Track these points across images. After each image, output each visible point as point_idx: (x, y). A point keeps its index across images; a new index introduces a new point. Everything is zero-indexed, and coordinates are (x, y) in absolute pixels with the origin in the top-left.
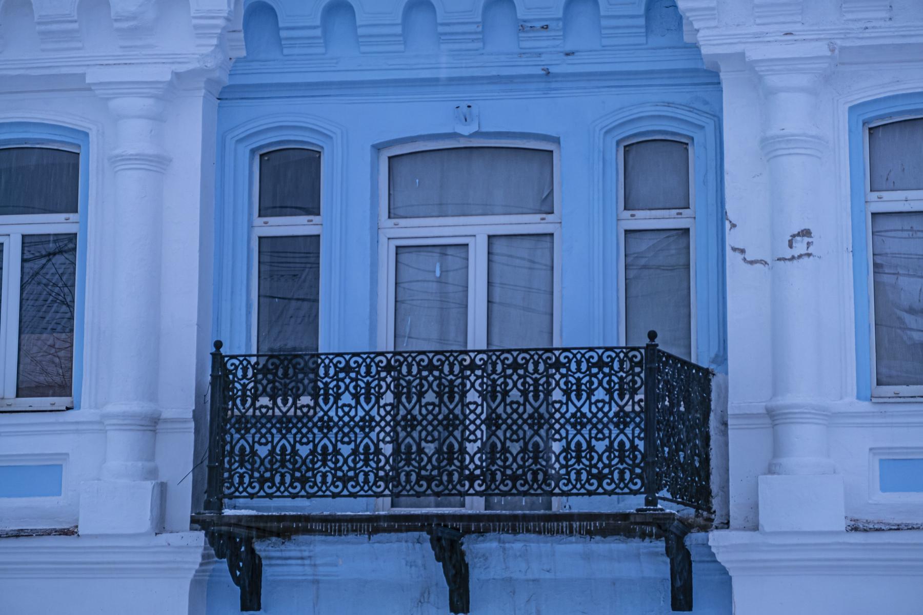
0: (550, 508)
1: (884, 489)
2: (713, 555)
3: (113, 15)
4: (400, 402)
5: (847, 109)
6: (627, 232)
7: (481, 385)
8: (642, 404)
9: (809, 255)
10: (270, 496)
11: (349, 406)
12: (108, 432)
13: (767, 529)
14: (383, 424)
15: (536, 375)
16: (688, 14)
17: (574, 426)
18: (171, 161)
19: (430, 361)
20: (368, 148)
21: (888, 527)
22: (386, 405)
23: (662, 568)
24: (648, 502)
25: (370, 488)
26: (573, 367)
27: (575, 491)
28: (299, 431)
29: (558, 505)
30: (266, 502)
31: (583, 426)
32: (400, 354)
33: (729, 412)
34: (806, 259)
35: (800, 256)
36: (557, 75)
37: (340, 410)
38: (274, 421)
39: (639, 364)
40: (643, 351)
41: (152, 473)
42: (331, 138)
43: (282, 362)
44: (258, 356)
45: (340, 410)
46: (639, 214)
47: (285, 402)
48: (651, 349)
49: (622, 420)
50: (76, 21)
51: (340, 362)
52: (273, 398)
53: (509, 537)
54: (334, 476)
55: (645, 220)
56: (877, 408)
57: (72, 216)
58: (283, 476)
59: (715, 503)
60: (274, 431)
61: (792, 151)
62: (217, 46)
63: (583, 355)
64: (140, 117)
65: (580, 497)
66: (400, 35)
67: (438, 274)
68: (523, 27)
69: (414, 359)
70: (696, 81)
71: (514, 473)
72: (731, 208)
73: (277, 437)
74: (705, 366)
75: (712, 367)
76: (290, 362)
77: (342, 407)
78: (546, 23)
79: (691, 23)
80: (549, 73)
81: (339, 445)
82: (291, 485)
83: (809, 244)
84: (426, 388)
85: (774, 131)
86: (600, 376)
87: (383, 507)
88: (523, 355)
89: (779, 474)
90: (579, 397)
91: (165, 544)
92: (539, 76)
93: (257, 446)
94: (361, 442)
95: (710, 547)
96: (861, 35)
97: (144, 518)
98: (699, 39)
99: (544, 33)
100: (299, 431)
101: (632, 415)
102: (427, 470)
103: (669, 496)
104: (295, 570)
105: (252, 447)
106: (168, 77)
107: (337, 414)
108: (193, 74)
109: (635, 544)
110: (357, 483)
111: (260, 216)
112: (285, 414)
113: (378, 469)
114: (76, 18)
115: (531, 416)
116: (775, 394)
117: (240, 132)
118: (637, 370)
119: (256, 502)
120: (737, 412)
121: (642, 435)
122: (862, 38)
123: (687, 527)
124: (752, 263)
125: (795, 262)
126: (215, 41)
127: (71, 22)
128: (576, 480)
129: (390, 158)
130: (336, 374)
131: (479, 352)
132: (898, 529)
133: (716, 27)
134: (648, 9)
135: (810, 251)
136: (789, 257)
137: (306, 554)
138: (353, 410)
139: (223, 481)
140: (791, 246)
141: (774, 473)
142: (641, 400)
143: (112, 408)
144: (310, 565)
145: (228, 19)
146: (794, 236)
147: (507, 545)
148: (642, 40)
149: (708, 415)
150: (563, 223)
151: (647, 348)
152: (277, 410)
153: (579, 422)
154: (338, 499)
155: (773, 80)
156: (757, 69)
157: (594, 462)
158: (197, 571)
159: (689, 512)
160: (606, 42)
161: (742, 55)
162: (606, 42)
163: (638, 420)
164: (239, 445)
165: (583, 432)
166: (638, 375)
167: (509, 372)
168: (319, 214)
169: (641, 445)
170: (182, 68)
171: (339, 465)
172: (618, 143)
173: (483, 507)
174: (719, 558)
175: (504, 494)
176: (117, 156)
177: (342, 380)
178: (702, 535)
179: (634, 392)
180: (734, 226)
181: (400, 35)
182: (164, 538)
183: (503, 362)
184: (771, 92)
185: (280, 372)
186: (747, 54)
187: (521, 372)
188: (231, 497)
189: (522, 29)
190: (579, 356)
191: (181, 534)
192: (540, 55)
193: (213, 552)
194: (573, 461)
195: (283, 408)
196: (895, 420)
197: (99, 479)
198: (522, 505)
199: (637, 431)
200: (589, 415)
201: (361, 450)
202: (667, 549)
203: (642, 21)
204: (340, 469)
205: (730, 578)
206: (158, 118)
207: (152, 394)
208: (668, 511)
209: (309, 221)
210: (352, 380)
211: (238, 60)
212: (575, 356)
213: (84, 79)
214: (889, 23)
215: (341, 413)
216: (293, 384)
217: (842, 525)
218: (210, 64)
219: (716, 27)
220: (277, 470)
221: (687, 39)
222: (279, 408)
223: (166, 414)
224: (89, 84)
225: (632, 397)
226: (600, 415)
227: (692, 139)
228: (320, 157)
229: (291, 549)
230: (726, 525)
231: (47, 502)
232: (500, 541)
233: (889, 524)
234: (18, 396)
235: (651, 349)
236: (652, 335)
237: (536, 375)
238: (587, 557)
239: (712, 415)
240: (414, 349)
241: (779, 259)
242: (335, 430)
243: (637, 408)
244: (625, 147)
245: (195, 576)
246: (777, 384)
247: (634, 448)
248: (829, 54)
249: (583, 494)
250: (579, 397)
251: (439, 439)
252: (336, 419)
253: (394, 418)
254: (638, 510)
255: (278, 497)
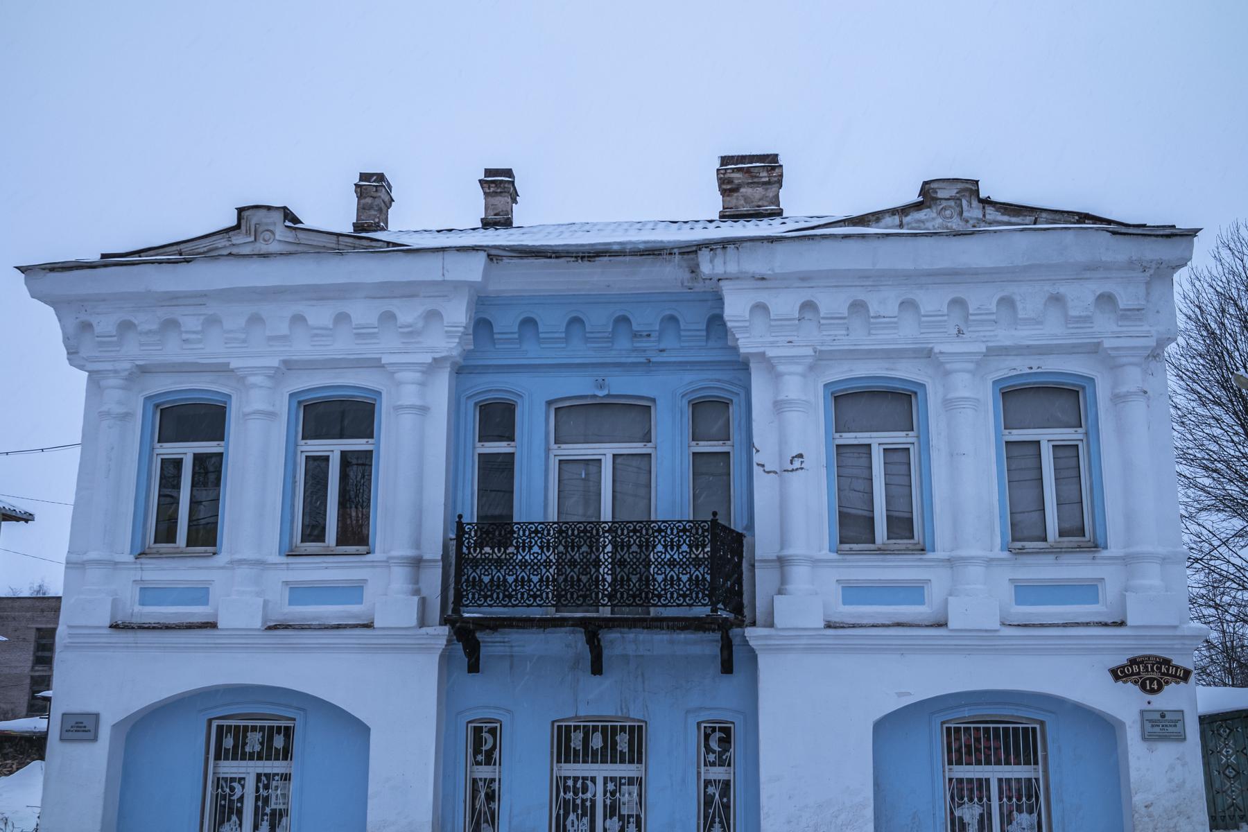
0: (649, 614)
1: (844, 603)
2: (747, 641)
3: (398, 324)
4: (617, 550)
5: (822, 386)
6: (694, 454)
7: (689, 541)
8: (709, 554)
9: (802, 468)
10: (490, 606)
11: (537, 553)
12: (392, 567)
13: (779, 626)
14: (631, 563)
15: (524, 538)
16: (732, 330)
17: (669, 566)
18: (429, 409)
19: (585, 527)
20: (544, 403)
21: (847, 626)
22: (608, 552)
23: (715, 649)
24: (712, 611)
25: (476, 602)
26: (669, 531)
27: (670, 604)
28: (508, 568)
29: (653, 612)
30: (489, 609)
31: (675, 566)
32: (617, 522)
33: (756, 558)
34: (800, 471)
35: (797, 469)
36: (654, 363)
37: (606, 555)
38: (493, 562)
39: (707, 530)
40: (709, 523)
41: (417, 592)
42: (521, 396)
43: (497, 527)
44: (613, 522)
45: (606, 555)
46: (701, 443)
47: (499, 551)
48: (714, 522)
49: (697, 562)
50: (376, 328)
51: (532, 528)
52: (492, 548)
53: (626, 630)
54: (528, 594)
55: (705, 447)
56: (841, 557)
57: (371, 441)
58: (498, 594)
59: (746, 611)
60: (493, 567)
61: (794, 409)
62: (458, 343)
63: (674, 525)
64: (413, 383)
65: (673, 608)
66: (517, 339)
67: (583, 476)
68: (636, 335)
69: (575, 526)
70: (736, 367)
71: (486, 593)
72: (756, 441)
73: (544, 570)
74: (740, 532)
75: (744, 532)
76: (502, 527)
77: (533, 554)
78: (648, 333)
79: (734, 335)
80: (650, 361)
81: (531, 576)
82: (503, 599)
83: (802, 462)
84: (533, 544)
85: (782, 397)
86: (685, 537)
87: (551, 612)
88: (639, 525)
89: (785, 594)
90: (524, 551)
91: (425, 633)
92: (645, 363)
93: (483, 576)
94: (694, 573)
95: (745, 637)
96: (832, 344)
97: (413, 621)
98: (739, 344)
99: (649, 339)
100: (508, 568)
101: (703, 560)
102: (583, 591)
103: (723, 607)
104: (498, 650)
105: (480, 577)
106: (430, 361)
107: (530, 558)
108: (444, 359)
109: (699, 635)
110: (542, 599)
111: (479, 441)
112: (499, 558)
113: (530, 590)
114: (995, 311)
115: (569, 561)
116: (782, 548)
117: (469, 393)
118: (706, 534)
119: (483, 609)
120: (760, 558)
121: (709, 572)
122: (831, 346)
123: (732, 625)
124: (769, 472)
125: (794, 473)
126: (457, 340)
127: (111, 336)
128: (645, 598)
129: (556, 409)
130: (530, 534)
131: (689, 522)
132: (853, 627)
133: (748, 337)
134: (708, 326)
135: (802, 466)
136: (790, 469)
137: (506, 640)
138: (540, 556)
139: (463, 597)
140: (792, 463)
141: (782, 594)
142: (708, 552)
143: (395, 553)
144: (509, 646)
145: (465, 328)
146: (793, 457)
147: (625, 635)
148: (704, 344)
149: (742, 560)
150: (658, 448)
151: (712, 521)
152: (494, 555)
153: (524, 564)
154: (516, 608)
155: (781, 368)
156: (772, 361)
157: (681, 587)
158: (443, 649)
159: (731, 616)
160: (683, 344)
161: (764, 353)
162: (683, 344)
163: (706, 563)
164: (472, 576)
165: (575, 570)
166: (607, 537)
167: (631, 534)
168: (514, 441)
169: (708, 577)
170: (437, 356)
171: (531, 588)
172: (689, 402)
173: (610, 613)
174: (751, 643)
175: (629, 605)
176: (399, 406)
177: (533, 538)
178: (739, 629)
179: (704, 546)
180: (758, 451)
181: (517, 339)
182: (424, 630)
183: (628, 529)
184: (947, 373)
185: (497, 533)
186: (767, 353)
187: (540, 535)
188: (467, 606)
189: (635, 336)
190: (672, 525)
191: (434, 628)
192: (645, 351)
193: (455, 638)
194: (669, 586)
195: (498, 553)
196: (850, 564)
197: (386, 595)
198: (637, 613)
199: (706, 569)
200: (678, 560)
201: (544, 579)
202: (722, 637)
203: (704, 333)
204: (532, 590)
205: (757, 655)
206: (422, 384)
207: (417, 544)
208: (724, 616)
209: (508, 445)
210: (663, 537)
211: (469, 351)
212: (670, 525)
213: (381, 361)
214: (847, 337)
215: (532, 557)
216: (504, 540)
217: (822, 625)
218: (455, 353)
219: (748, 337)
220: (495, 591)
221: (730, 343)
222: (496, 554)
223: (426, 557)
224: (384, 364)
225: (703, 550)
226: (685, 560)
227: (732, 401)
228: (514, 408)
229: (497, 637)
230: (753, 624)
231: (355, 608)
232: (621, 633)
233: (847, 624)
234: (337, 545)
235: (714, 522)
236: (715, 514)
237: (524, 538)
238: (672, 642)
239: (744, 560)
240: (576, 520)
241: (785, 471)
242: (529, 567)
243: (706, 556)
244: (693, 404)
245: (442, 652)
246: (783, 543)
247: (704, 579)
248: (813, 354)
249: (674, 606)
250: (524, 551)
251: (640, 573)
252: (529, 561)
253: (613, 560)
254: (707, 615)
255: (495, 606)
